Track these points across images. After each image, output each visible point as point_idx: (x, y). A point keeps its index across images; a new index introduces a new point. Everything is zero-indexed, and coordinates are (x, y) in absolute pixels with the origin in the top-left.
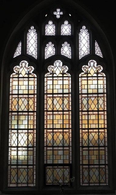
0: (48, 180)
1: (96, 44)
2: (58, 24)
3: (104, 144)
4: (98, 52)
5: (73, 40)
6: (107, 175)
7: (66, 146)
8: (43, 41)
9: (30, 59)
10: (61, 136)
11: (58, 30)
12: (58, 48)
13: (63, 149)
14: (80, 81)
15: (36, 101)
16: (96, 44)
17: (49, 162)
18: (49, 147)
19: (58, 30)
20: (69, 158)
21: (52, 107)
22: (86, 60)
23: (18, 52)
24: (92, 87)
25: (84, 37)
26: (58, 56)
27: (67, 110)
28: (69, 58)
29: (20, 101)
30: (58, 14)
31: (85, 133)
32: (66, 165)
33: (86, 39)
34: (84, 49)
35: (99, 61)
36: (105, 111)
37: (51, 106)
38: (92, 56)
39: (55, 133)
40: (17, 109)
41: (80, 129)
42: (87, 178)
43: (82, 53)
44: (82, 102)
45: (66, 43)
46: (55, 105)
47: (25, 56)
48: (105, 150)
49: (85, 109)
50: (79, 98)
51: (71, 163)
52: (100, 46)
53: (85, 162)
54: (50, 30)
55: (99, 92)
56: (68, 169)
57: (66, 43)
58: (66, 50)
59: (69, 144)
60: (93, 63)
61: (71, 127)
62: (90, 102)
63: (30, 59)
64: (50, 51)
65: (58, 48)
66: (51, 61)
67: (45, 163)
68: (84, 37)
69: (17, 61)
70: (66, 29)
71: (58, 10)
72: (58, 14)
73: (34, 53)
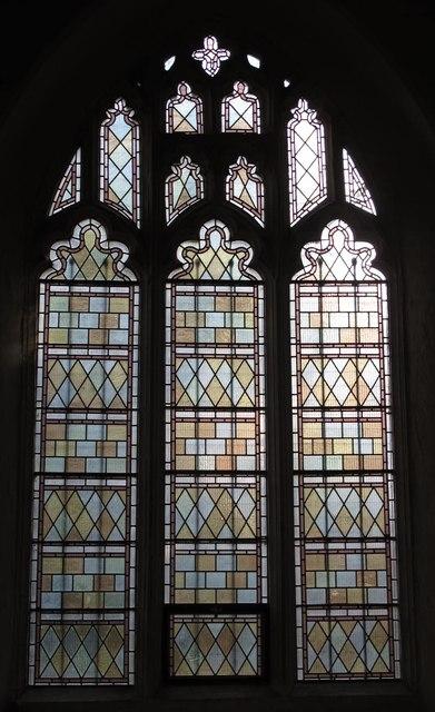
0: (176, 665)
1: (347, 161)
2: (212, 93)
3: (124, 533)
4: (356, 190)
5: (269, 153)
6: (33, 642)
7: (333, 538)
8: (159, 153)
9: (115, 223)
10: (354, 500)
11: (211, 114)
12: (215, 180)
13: (326, 549)
14: (292, 297)
15: (135, 373)
16: (347, 161)
17: (184, 598)
18: (314, 540)
19: (211, 114)
20: (172, 576)
21: (321, 392)
22: (313, 226)
23: (68, 193)
24: (339, 320)
25: (306, 137)
26: (214, 205)
27: (250, 405)
28: (370, 211)
29: (330, 369)
30: (211, 56)
31: (185, 488)
32: (247, 609)
33: (297, 140)
34: (307, 185)
35: (362, 226)
36: (260, 409)
37: (318, 391)
38: (334, 206)
39: (205, 488)
40: (320, 398)
41: (36, 474)
42: (243, 658)
43: (301, 201)
44: (48, 373)
45: (186, 161)
46: (331, 385)
47: (93, 205)
48: (386, 551)
49: (312, 402)
50: (164, 360)
51: (265, 601)
52: (359, 165)
53: (315, 597)
54: (184, 113)
55: (75, 341)
56: (254, 627)
57: (186, 161)
58: (245, 188)
59: (128, 533)
60: (337, 234)
61: (134, 471)
62: (330, 374)
63: (115, 223)
64: (184, 185)
65: (215, 180)
66: (190, 224)
67: (167, 601)
68: (306, 137)
69: (63, 226)
70: (241, 112)
71: (211, 43)
72: (211, 56)
73: (128, 202)
